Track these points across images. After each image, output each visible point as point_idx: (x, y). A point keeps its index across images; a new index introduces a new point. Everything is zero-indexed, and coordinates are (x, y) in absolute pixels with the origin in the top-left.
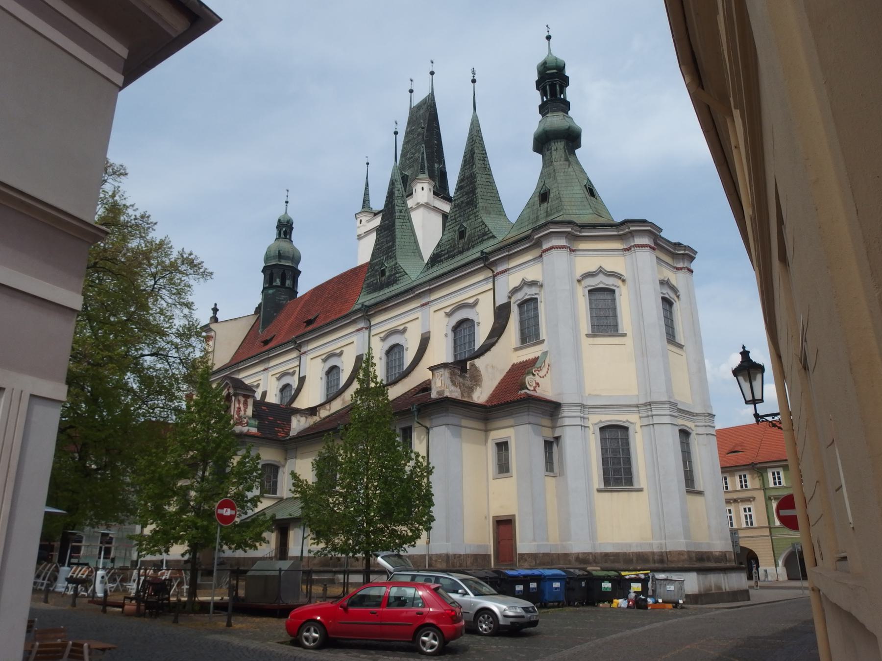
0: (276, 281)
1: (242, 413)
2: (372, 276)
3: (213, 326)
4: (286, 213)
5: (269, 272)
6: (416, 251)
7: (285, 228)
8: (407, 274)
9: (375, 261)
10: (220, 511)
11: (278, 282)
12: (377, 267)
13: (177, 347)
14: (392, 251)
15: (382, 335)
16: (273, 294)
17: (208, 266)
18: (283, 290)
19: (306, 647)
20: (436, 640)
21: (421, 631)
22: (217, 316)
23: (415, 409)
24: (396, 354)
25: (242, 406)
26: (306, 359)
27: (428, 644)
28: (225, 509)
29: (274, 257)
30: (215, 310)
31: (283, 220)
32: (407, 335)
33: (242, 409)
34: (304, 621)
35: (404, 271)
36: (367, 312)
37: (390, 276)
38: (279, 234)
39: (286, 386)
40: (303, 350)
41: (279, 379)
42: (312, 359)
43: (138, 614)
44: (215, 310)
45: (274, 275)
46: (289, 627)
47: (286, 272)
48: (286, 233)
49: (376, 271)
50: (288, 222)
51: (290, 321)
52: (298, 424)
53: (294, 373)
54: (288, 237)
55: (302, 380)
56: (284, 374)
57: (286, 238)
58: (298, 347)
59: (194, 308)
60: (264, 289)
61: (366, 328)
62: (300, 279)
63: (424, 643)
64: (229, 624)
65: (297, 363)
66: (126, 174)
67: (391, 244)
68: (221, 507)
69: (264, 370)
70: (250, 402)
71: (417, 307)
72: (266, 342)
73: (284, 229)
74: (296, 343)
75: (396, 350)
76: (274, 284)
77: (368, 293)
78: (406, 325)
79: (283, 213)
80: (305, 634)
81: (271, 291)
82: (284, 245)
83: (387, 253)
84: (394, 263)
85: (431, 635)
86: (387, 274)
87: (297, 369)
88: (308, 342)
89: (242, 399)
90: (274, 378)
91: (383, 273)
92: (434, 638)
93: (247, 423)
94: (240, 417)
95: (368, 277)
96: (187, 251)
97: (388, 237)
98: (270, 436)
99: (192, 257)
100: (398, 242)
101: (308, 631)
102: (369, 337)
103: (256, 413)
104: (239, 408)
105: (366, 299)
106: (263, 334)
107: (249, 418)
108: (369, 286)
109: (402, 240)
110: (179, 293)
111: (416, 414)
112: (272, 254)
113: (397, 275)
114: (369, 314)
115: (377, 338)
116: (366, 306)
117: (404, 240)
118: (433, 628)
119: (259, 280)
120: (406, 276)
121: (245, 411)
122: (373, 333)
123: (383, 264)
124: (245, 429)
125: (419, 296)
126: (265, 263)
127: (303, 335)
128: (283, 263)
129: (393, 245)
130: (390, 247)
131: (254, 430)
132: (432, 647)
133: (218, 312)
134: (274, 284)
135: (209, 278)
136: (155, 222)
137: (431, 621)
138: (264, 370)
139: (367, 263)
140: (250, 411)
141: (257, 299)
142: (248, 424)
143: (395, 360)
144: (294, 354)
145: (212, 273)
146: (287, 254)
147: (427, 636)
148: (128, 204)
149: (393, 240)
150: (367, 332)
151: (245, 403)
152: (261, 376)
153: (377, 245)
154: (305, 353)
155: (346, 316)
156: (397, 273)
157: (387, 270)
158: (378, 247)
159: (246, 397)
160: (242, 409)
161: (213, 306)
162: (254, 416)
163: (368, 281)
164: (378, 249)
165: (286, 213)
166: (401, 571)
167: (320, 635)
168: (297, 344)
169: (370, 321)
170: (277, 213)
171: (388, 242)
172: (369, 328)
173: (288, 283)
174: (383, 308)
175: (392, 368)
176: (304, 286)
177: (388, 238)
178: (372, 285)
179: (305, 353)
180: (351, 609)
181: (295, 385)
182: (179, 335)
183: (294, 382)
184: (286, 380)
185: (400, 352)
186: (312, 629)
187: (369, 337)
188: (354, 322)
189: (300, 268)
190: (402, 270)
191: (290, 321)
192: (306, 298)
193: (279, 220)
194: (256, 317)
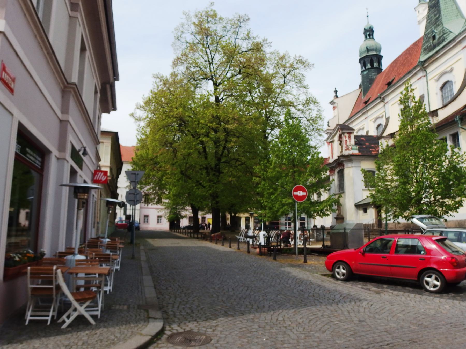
0: (367, 65)
1: (348, 143)
2: (428, 41)
3: (335, 101)
4: (368, 23)
5: (362, 62)
6: (459, 14)
7: (369, 33)
8: (451, 32)
9: (428, 32)
10: (295, 193)
11: (369, 66)
12: (429, 36)
13: (303, 112)
14: (439, 21)
15: (436, 78)
16: (367, 74)
17: (311, 61)
18: (372, 70)
19: (338, 279)
20: (438, 281)
21: (424, 273)
22: (337, 95)
23: (458, 119)
24: (447, 88)
25: (347, 139)
26: (388, 106)
27: (431, 284)
28: (299, 192)
29: (364, 52)
30: (336, 92)
31: (367, 28)
32: (454, 72)
33: (348, 140)
34: (335, 261)
35: (450, 31)
36: (423, 65)
37: (440, 37)
38: (366, 37)
39: (379, 125)
40: (386, 101)
41: (375, 122)
42: (392, 105)
43: (261, 254)
44: (336, 92)
45: (366, 62)
46: (327, 264)
47: (373, 58)
48: (369, 35)
49: (429, 38)
50: (370, 28)
51: (379, 87)
52: (384, 144)
53: (382, 117)
54: (371, 37)
55: (388, 119)
56: (377, 118)
57: (370, 38)
58: (383, 100)
59: (308, 87)
60: (362, 72)
61: (424, 76)
62: (383, 61)
63: (428, 283)
64: (305, 261)
65: (384, 110)
66: (249, 19)
67: (437, 16)
68: (296, 190)
69: (366, 118)
70: (352, 136)
71: (460, 51)
72: (366, 103)
73: (368, 33)
74: (381, 98)
75: (447, 85)
76: (367, 68)
77: (425, 54)
78: (453, 66)
79: (366, 23)
80: (337, 270)
81: (365, 73)
82: (370, 43)
83: (436, 23)
84: (441, 28)
85: (434, 276)
86: (437, 37)
87: (384, 114)
88: (388, 95)
89: (347, 135)
90: (372, 122)
91: (434, 37)
92: (437, 279)
93: (352, 149)
94: (347, 146)
95: (424, 44)
96: (298, 55)
97: (435, 11)
98: (367, 154)
99: (301, 58)
100: (443, 13)
101: (339, 268)
102: (427, 81)
103: (357, 142)
104: (346, 141)
105: (423, 58)
106: (364, 99)
107: (353, 146)
108: (425, 49)
109: (446, 10)
110: (300, 81)
111: (459, 122)
112: (363, 50)
113: (445, 36)
114: (424, 66)
115: (433, 81)
116: (421, 62)
117: (448, 10)
118: (431, 271)
119: (358, 67)
120: (451, 34)
121: (350, 142)
122: (429, 78)
123: (433, 32)
124: (351, 152)
125: (460, 42)
126: (360, 56)
127: (384, 92)
128: (371, 53)
129: (440, 16)
130: (437, 19)
131: (356, 152)
132: (435, 286)
133: (337, 93)
134: (367, 68)
135: (312, 67)
136: (271, 41)
137: (435, 266)
138: (366, 118)
139: (423, 37)
140: (353, 141)
141: (359, 80)
142: (352, 149)
143: (448, 92)
144: (382, 104)
145: (313, 65)
146: (372, 48)
147: (430, 277)
148: (255, 36)
149: (439, 12)
150: (425, 78)
151: (350, 137)
152: (365, 122)
153: (428, 20)
154: (387, 102)
155: (410, 72)
156: (444, 34)
157: (437, 35)
158: (429, 21)
159: (350, 133)
160: (348, 140)
161: (334, 90)
162: (356, 144)
163: (424, 47)
164: (429, 22)
165: (368, 23)
166: (432, 228)
167: (347, 271)
168: (382, 98)
169: (426, 71)
170: (364, 25)
171: (435, 15)
172: (426, 76)
173: (375, 65)
174: (434, 59)
175: (446, 98)
176: (385, 64)
177: (436, 13)
178: (428, 48)
179: (387, 102)
180: (368, 254)
181: (384, 124)
182: (304, 105)
183: (383, 122)
184: (378, 122)
185: (450, 86)
186: (341, 267)
187: (427, 81)
188: (415, 74)
189: (382, 54)
190: (448, 31)
191: (379, 87)
192: (387, 71)
193: (365, 29)
194: (360, 90)
